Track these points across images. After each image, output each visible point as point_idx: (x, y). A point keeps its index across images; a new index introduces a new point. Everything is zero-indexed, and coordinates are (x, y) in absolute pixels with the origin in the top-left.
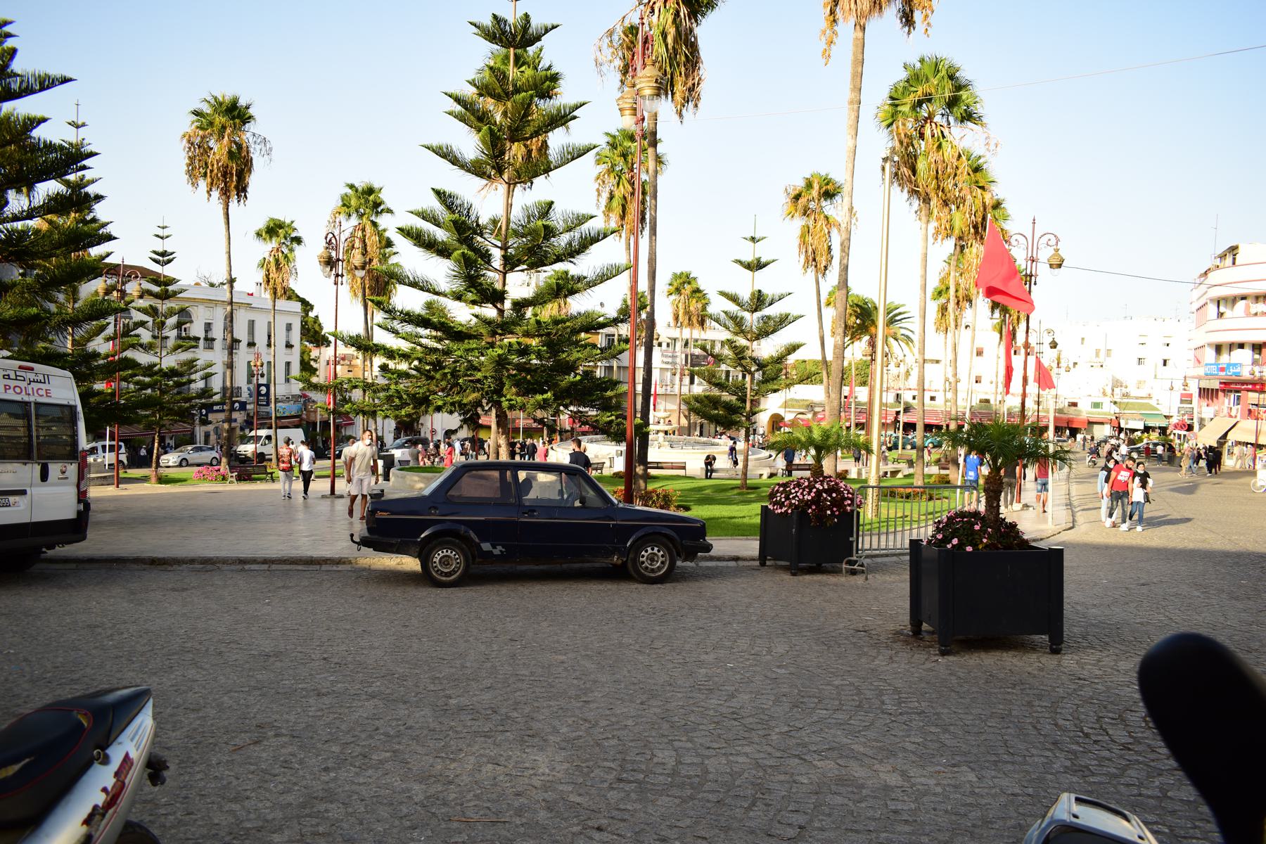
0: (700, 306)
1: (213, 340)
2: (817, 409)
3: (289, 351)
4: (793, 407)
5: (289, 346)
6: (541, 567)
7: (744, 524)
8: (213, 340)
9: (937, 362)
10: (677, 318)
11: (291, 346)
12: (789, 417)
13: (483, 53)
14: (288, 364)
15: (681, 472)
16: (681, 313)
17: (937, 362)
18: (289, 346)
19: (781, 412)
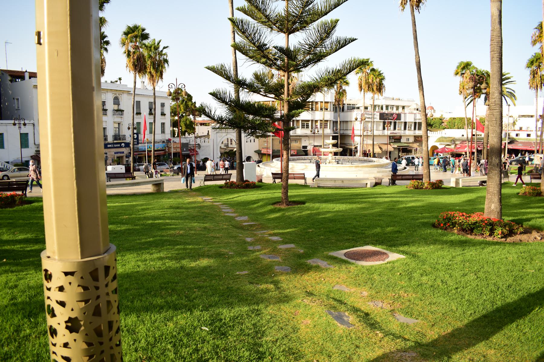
0: (378, 80)
1: (107, 110)
2: (457, 143)
3: (163, 117)
4: (443, 141)
5: (163, 114)
6: (288, 230)
7: (372, 214)
8: (107, 110)
9: (532, 116)
10: (361, 87)
11: (165, 115)
12: (440, 147)
13: (458, 76)
14: (163, 124)
15: (302, 182)
16: (363, 85)
17: (532, 116)
18: (163, 114)
19: (437, 144)
